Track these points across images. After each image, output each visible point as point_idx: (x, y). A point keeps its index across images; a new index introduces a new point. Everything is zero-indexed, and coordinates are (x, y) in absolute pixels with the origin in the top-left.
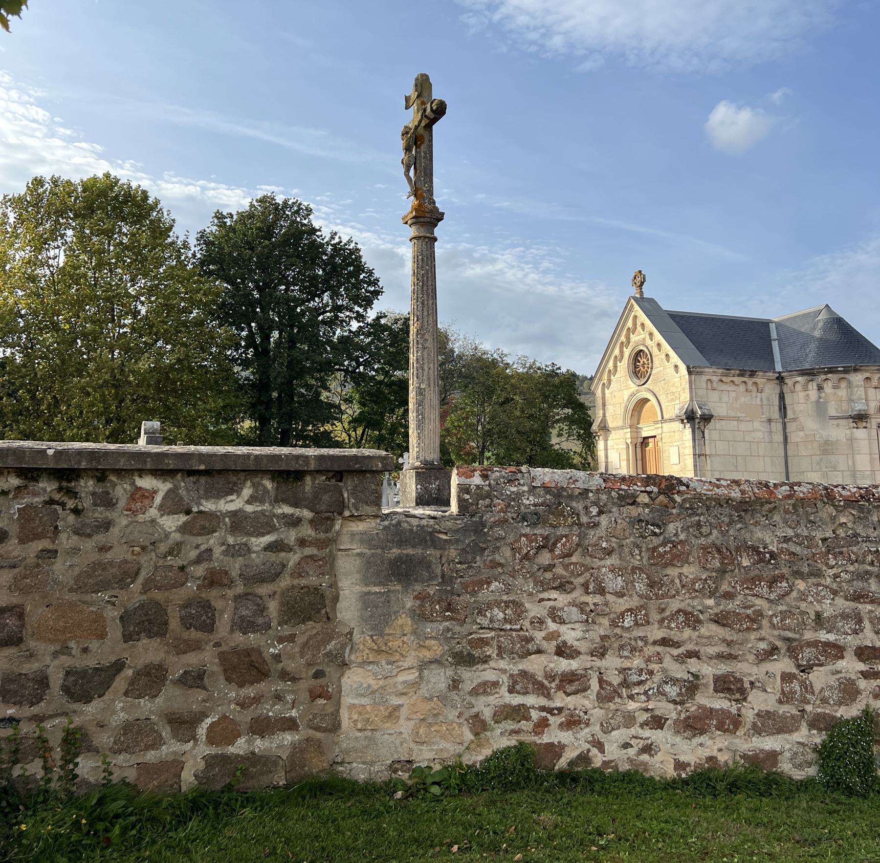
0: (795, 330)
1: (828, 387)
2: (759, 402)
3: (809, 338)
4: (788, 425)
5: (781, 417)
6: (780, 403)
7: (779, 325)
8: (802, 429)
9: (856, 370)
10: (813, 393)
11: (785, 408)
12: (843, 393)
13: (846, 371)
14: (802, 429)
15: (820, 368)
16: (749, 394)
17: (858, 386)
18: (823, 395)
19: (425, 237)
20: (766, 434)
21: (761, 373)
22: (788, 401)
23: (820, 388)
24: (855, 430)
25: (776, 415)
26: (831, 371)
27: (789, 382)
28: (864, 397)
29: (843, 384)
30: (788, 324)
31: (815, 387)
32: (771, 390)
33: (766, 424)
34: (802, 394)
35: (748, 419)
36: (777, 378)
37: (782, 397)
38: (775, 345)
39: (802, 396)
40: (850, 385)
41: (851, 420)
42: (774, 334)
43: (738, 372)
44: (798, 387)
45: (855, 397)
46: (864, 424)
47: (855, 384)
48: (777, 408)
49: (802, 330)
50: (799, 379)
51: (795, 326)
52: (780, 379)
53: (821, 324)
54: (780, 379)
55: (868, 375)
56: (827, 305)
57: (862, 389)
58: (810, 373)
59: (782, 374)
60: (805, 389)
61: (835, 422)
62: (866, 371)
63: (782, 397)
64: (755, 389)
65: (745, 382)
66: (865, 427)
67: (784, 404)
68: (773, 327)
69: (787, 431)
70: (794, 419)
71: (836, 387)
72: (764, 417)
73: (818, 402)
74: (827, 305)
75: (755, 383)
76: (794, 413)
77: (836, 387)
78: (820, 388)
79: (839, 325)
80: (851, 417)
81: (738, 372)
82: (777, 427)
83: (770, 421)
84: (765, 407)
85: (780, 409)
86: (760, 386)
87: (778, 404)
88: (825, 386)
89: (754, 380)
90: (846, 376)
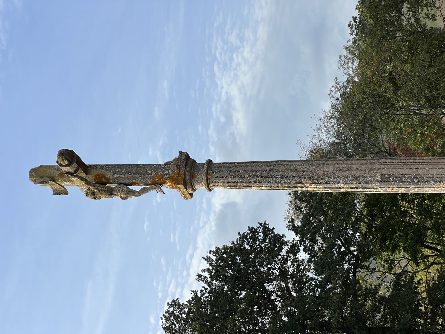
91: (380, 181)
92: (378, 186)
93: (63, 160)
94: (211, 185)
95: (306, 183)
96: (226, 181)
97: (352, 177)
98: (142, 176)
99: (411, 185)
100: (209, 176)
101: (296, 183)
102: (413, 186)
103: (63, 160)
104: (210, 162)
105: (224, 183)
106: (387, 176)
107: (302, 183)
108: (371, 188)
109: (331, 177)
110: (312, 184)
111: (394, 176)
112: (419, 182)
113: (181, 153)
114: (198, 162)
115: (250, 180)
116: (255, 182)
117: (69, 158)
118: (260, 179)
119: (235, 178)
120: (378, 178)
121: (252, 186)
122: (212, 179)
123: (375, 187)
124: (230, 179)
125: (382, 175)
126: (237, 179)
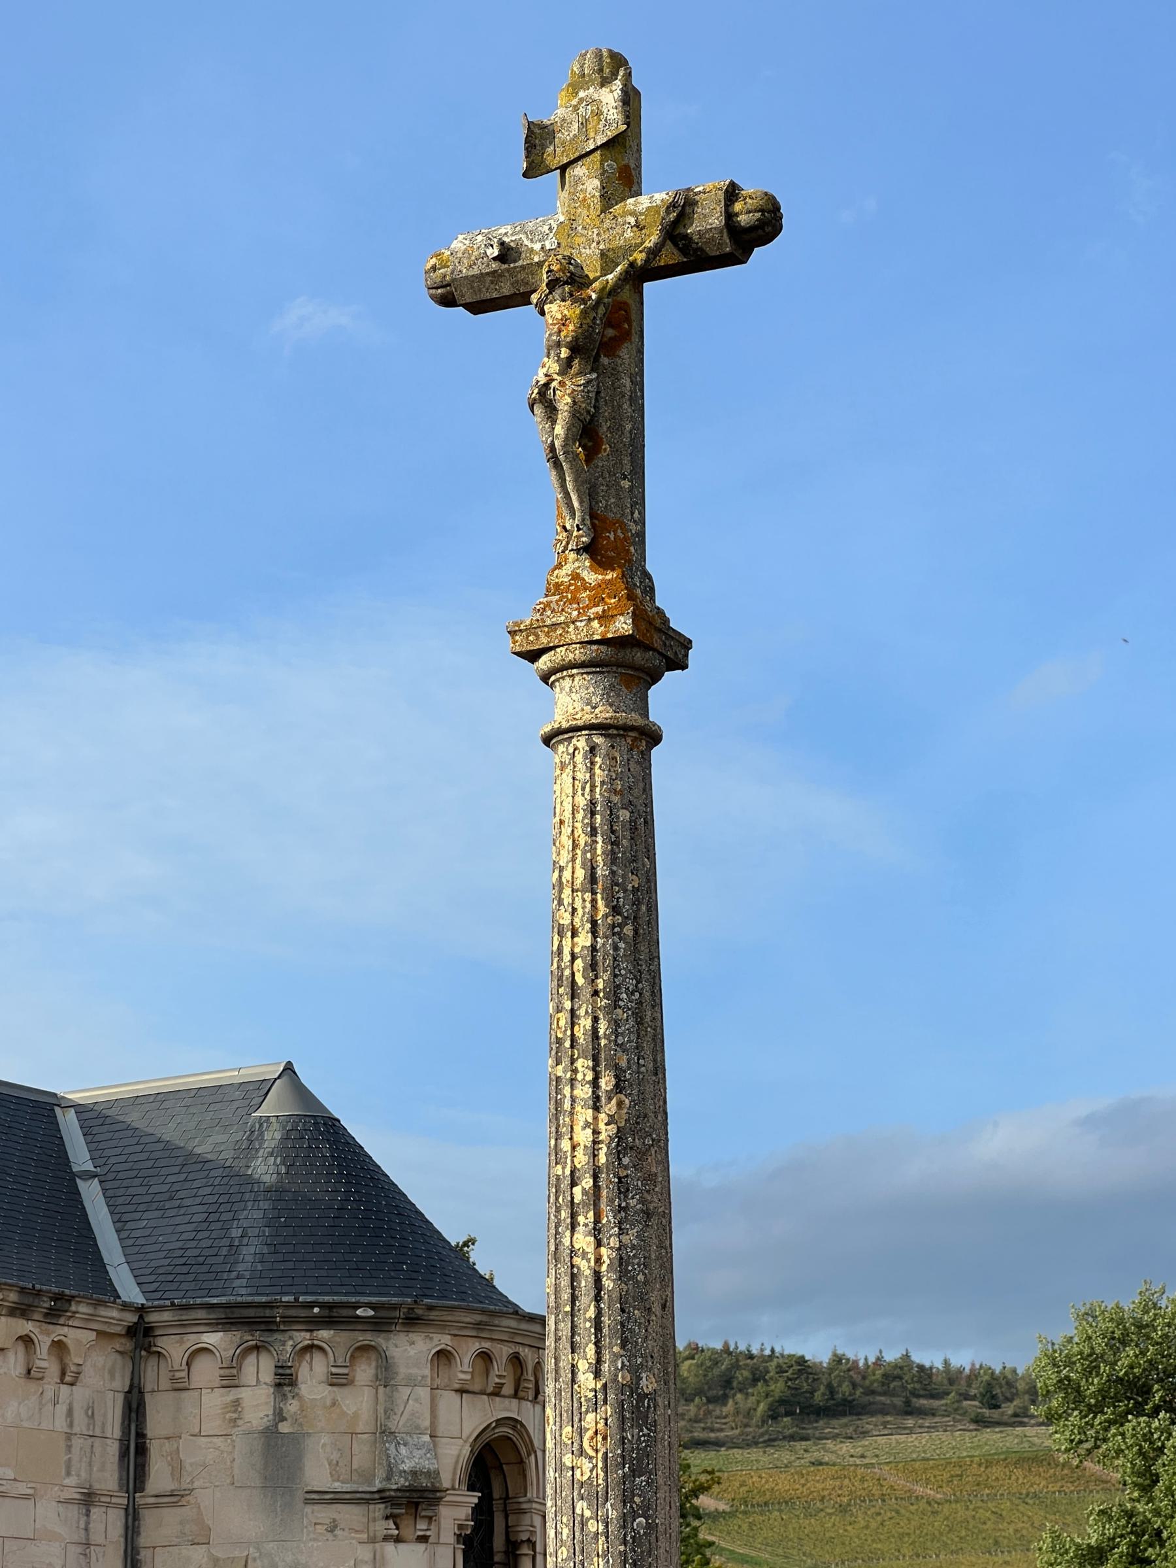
0: (169, 1147)
1: (312, 1378)
2: (61, 1424)
3: (235, 1185)
4: (149, 1519)
5: (124, 1485)
6: (126, 1430)
7: (94, 1118)
8: (202, 1539)
9: (412, 1321)
10: (257, 1398)
11: (142, 1450)
12: (359, 1402)
13: (380, 1324)
14: (202, 1539)
15: (297, 1305)
16: (33, 1386)
17: (412, 1383)
18: (292, 1407)
19: (626, 728)
20: (74, 1550)
21: (83, 1308)
22: (157, 1421)
23: (285, 1380)
24: (390, 1547)
25: (108, 1478)
26: (333, 1317)
27: (174, 1348)
28: (427, 1423)
29: (365, 1372)
30: (134, 1118)
31: (267, 1374)
32: (102, 1375)
33: (74, 1511)
34: (214, 1401)
35: (22, 1489)
36: (131, 1332)
37: (134, 1407)
38: (92, 1194)
39: (216, 1403)
40: (386, 1376)
41: (379, 1509)
42: (80, 1156)
43: (13, 1296)
44: (206, 1371)
45: (399, 1423)
46: (421, 1525)
47: (403, 1371)
48: (113, 1449)
49: (203, 1149)
50: (213, 1339)
51: (170, 1132)
52: (140, 1336)
53: (273, 1136)
54: (140, 1336)
55: (444, 1340)
56: (289, 1068)
57: (424, 1393)
58: (255, 1322)
59: (152, 1318)
60: (231, 1380)
61: (325, 1514)
62: (442, 1327)
63: (134, 1407)
64: (53, 1369)
65: (27, 1341)
66: (423, 1539)
67: (141, 1435)
68: (69, 1123)
69: (143, 1541)
70: (176, 1498)
71: (338, 1380)
72: (71, 1486)
73: (270, 1434)
74: (289, 1068)
75: (59, 1347)
76: (177, 1468)
77: (338, 1380)
78: (285, 1380)
79: (323, 1140)
80: (382, 1496)
81: (13, 1296)
82: (108, 1524)
83: (88, 1499)
84: (77, 1442)
85: (124, 1454)
86: (75, 1358)
87: (117, 1434)
88: (303, 1373)
89: (58, 1333)
90: (380, 1340)
91: (633, 1388)
92: (615, 1380)
93: (762, 211)
94: (599, 740)
95: (620, 1104)
96: (616, 799)
97: (646, 1283)
98: (626, 484)
99: (619, 1505)
100: (635, 739)
101: (617, 1067)
102: (613, 1514)
103: (762, 211)
104: (653, 737)
105: (609, 791)
106: (651, 1415)
107: (618, 1088)
108: (598, 1353)
109: (642, 1201)
110: (613, 1129)
111: (652, 1441)
112: (633, 1538)
113: (686, 644)
114: (654, 692)
115: (625, 891)
116: (615, 910)
117: (760, 232)
118: (628, 930)
119: (628, 834)
120: (643, 1382)
121: (594, 893)
122: (624, 744)
123: (605, 1367)
124: (624, 815)
125: (652, 1397)
126: (625, 842)
